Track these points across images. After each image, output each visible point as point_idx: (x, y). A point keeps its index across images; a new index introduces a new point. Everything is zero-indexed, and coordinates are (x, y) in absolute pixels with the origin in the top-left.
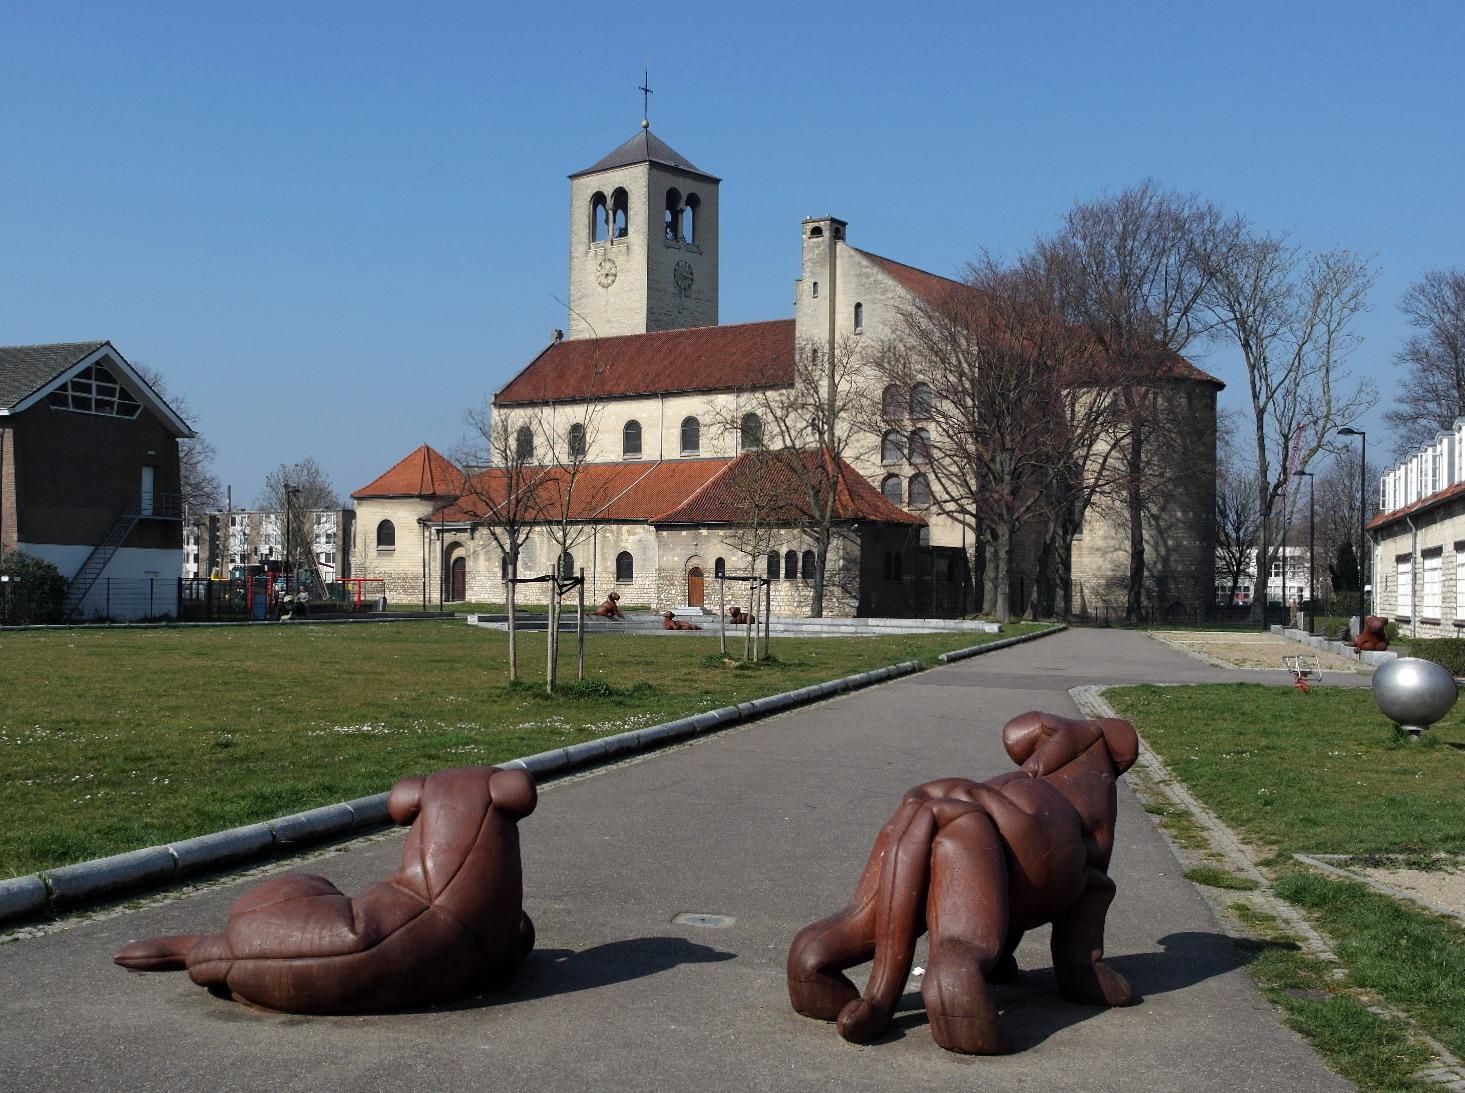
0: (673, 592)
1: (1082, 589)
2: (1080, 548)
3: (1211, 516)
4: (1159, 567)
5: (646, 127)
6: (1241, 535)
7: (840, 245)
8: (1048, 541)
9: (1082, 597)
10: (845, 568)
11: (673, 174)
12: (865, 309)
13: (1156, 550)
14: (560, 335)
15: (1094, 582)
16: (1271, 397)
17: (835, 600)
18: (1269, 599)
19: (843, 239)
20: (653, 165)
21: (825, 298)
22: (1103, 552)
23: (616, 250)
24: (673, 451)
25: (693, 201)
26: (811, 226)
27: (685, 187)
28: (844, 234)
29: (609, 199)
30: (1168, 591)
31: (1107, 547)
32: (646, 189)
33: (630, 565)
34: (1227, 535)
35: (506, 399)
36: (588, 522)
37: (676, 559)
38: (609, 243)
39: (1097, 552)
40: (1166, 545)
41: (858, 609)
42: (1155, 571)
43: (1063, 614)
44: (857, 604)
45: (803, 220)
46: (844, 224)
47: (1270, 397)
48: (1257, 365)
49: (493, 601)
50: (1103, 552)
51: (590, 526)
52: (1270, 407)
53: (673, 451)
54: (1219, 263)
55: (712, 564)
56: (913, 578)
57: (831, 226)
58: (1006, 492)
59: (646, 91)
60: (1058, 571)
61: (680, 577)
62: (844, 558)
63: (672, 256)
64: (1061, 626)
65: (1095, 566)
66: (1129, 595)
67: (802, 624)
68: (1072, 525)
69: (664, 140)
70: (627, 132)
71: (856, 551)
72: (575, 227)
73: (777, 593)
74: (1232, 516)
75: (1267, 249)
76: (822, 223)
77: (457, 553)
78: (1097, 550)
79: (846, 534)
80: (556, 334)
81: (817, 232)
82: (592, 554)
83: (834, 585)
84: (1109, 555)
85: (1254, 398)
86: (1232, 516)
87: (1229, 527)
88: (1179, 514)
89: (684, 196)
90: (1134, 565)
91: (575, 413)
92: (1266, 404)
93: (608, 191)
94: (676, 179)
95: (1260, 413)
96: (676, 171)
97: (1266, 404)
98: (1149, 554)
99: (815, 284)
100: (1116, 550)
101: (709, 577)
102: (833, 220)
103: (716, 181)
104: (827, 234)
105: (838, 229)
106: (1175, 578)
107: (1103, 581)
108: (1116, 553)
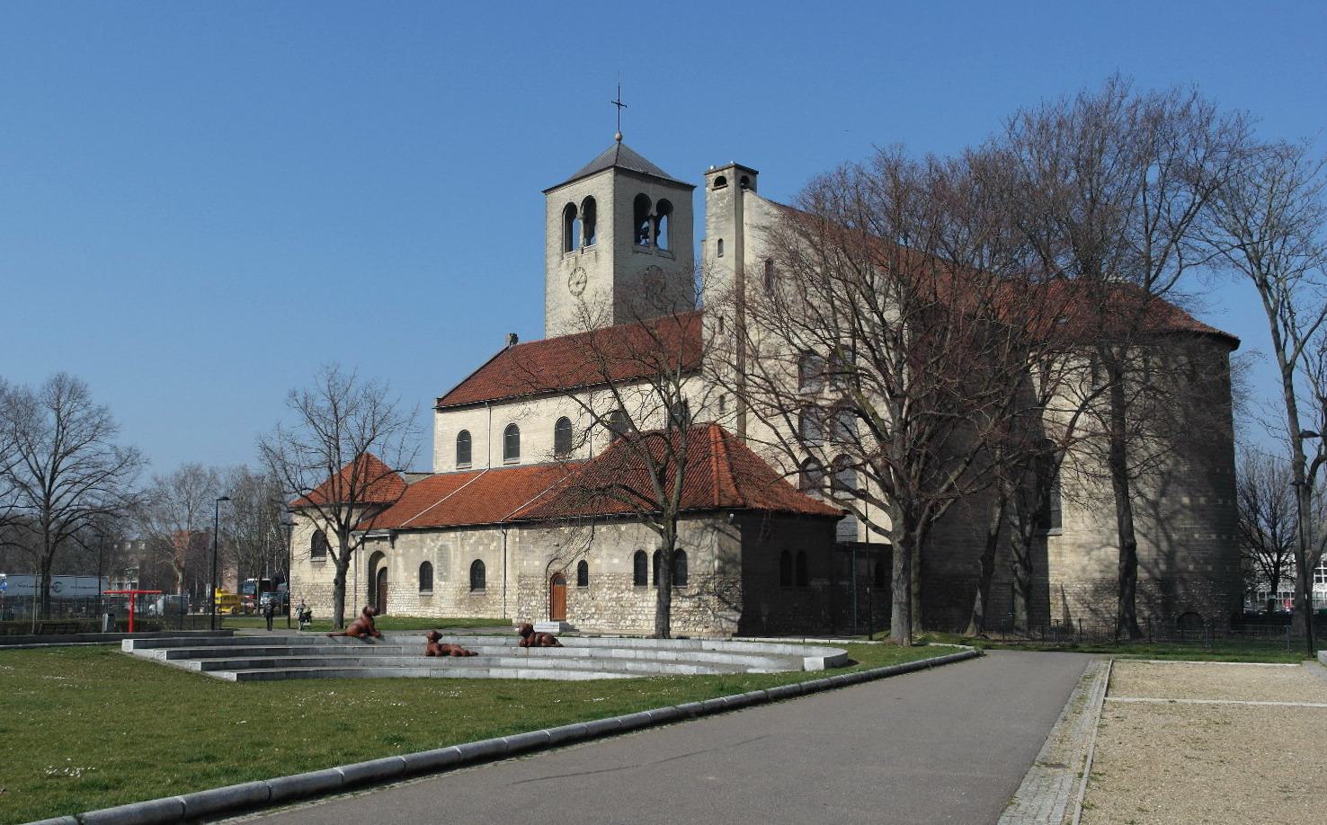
0: (534, 603)
1: (1064, 596)
2: (1059, 545)
3: (1230, 503)
4: (1163, 567)
5: (619, 140)
6: (1278, 531)
7: (748, 196)
8: (993, 532)
9: (1065, 605)
10: (721, 571)
11: (642, 181)
12: (725, 243)
13: (1158, 546)
14: (514, 338)
15: (1077, 587)
16: (1301, 350)
17: (710, 612)
18: (1316, 607)
19: (753, 189)
20: (619, 171)
21: (731, 256)
22: (1087, 549)
23: (586, 259)
24: (498, 461)
25: (665, 207)
26: (714, 176)
27: (655, 193)
28: (755, 184)
29: (579, 209)
30: (1176, 597)
31: (1093, 543)
32: (611, 195)
33: (431, 570)
34: (1259, 531)
35: (445, 406)
36: (496, 526)
37: (537, 563)
38: (580, 252)
39: (1078, 551)
40: (1169, 539)
41: (741, 623)
42: (1156, 571)
43: (1025, 628)
44: (738, 618)
45: (706, 170)
46: (755, 173)
47: (1299, 350)
48: (1279, 310)
49: (411, 614)
50: (1087, 549)
51: (500, 531)
52: (1300, 361)
53: (498, 461)
54: (1223, 187)
55: (574, 568)
56: (827, 583)
57: (736, 174)
58: (897, 456)
59: (619, 104)
60: (1015, 574)
61: (541, 589)
62: (719, 558)
63: (641, 261)
64: (971, 649)
65: (1078, 567)
66: (1120, 603)
67: (611, 648)
68: (1045, 520)
69: (635, 149)
70: (605, 149)
71: (735, 547)
72: (549, 240)
73: (645, 604)
74: (1265, 509)
75: (1284, 153)
76: (726, 171)
77: (381, 564)
78: (1079, 546)
79: (722, 527)
80: (510, 338)
81: (721, 182)
82: (502, 561)
83: (709, 593)
84: (1095, 553)
85: (1278, 351)
86: (1265, 509)
87: (1262, 523)
88: (1186, 500)
89: (653, 208)
90: (1124, 563)
91: (503, 415)
92: (1295, 357)
93: (578, 202)
94: (645, 184)
95: (1288, 369)
96: (645, 177)
97: (1295, 357)
98: (1143, 547)
99: (720, 241)
100: (1104, 546)
101: (572, 583)
102: (737, 167)
103: (690, 188)
104: (731, 183)
105: (746, 178)
106: (1184, 581)
107: (1089, 586)
108: (1103, 550)
